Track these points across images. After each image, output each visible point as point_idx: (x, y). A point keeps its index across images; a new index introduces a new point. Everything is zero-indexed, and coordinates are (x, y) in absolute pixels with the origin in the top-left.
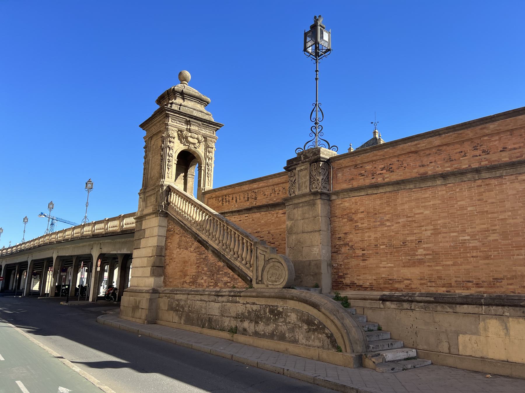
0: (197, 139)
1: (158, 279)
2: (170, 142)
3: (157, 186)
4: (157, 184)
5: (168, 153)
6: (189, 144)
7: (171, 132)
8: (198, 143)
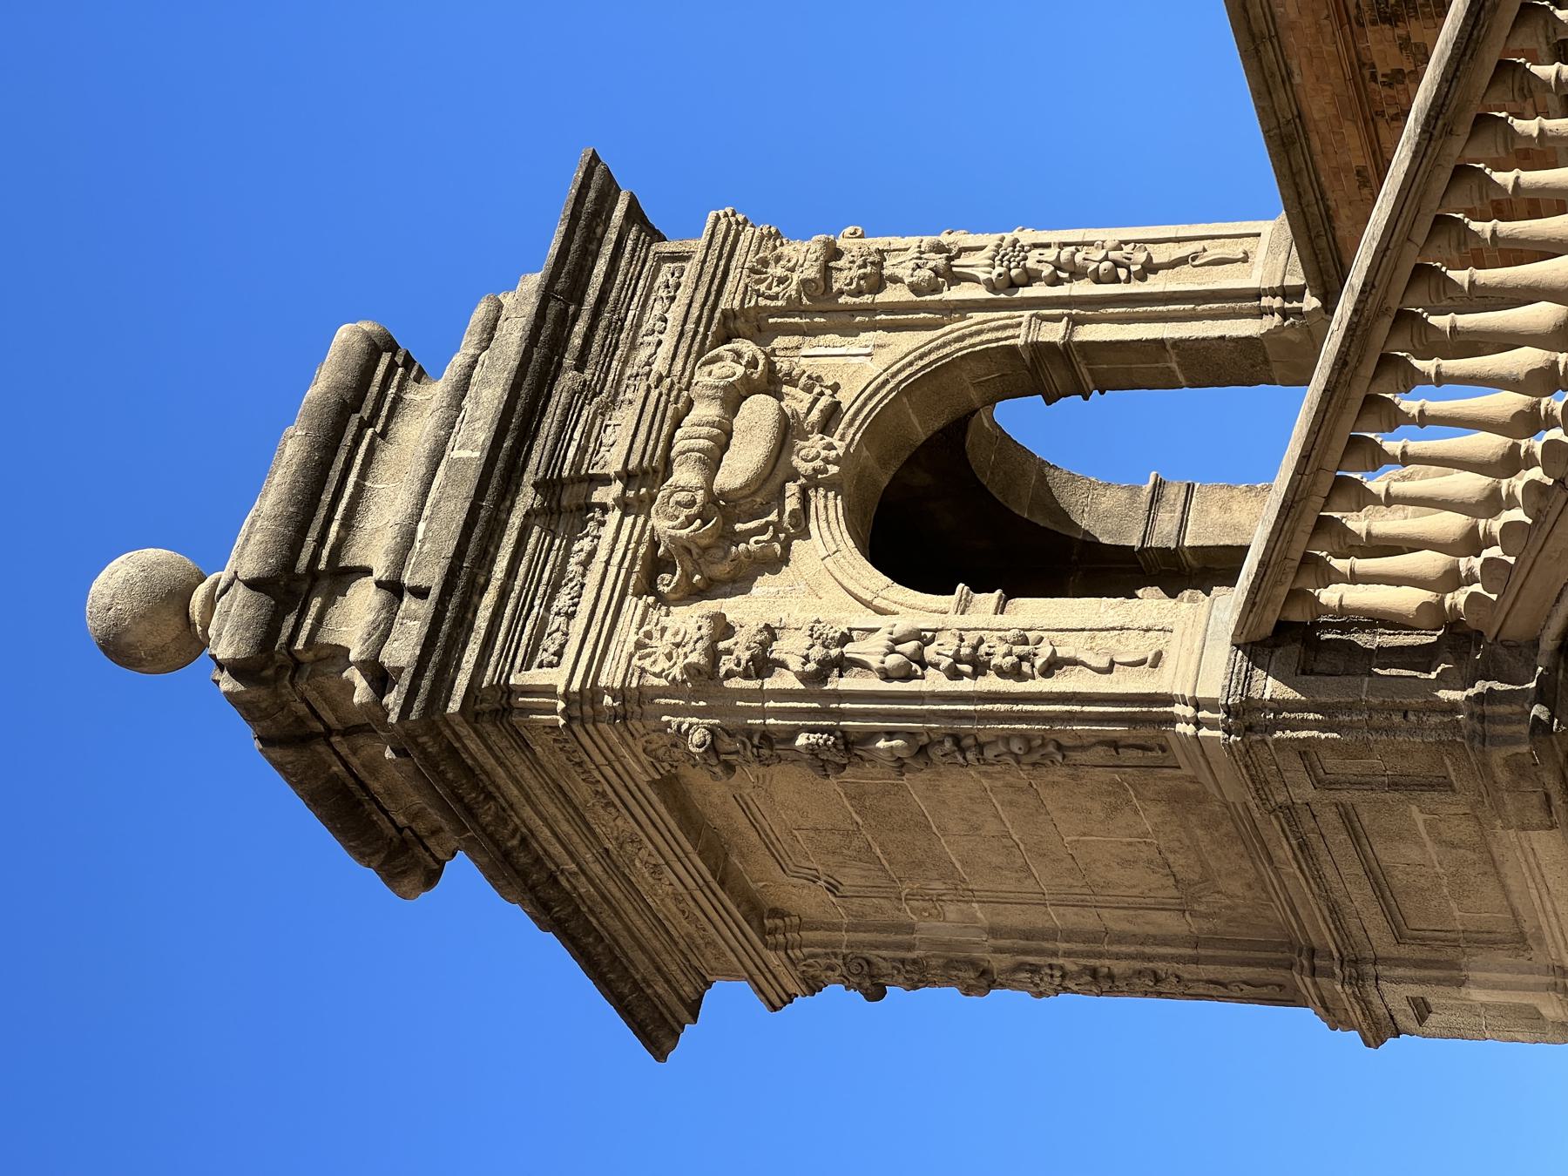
0: (733, 398)
2: (762, 665)
3: (1259, 784)
4: (1235, 790)
5: (886, 676)
6: (794, 475)
7: (663, 664)
8: (779, 397)
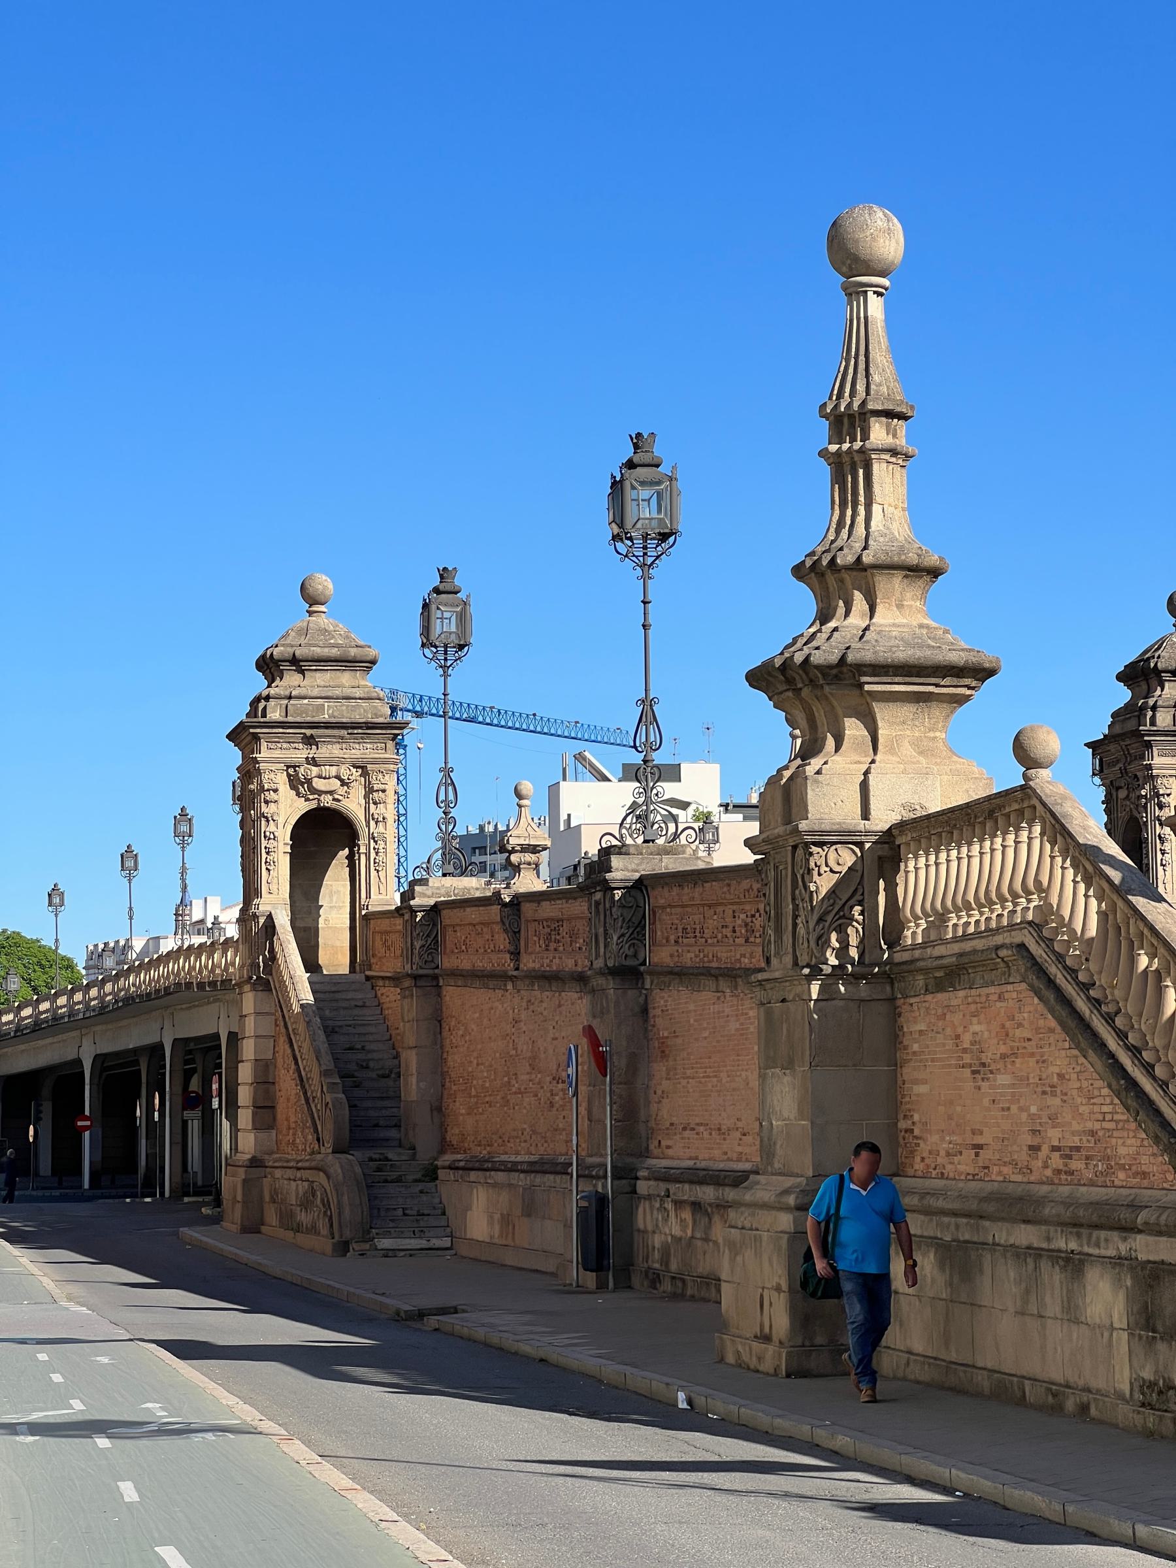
0: (338, 777)
1: (263, 1135)
2: (267, 802)
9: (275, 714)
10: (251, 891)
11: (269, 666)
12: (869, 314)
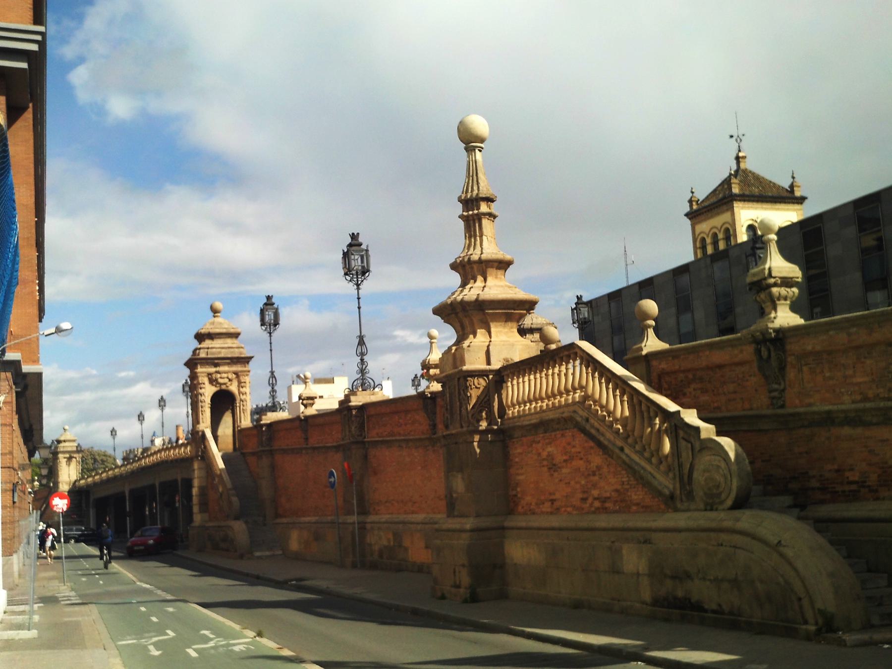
0: (228, 378)
2: (201, 388)
9: (203, 355)
10: (196, 421)
11: (200, 337)
12: (477, 158)
